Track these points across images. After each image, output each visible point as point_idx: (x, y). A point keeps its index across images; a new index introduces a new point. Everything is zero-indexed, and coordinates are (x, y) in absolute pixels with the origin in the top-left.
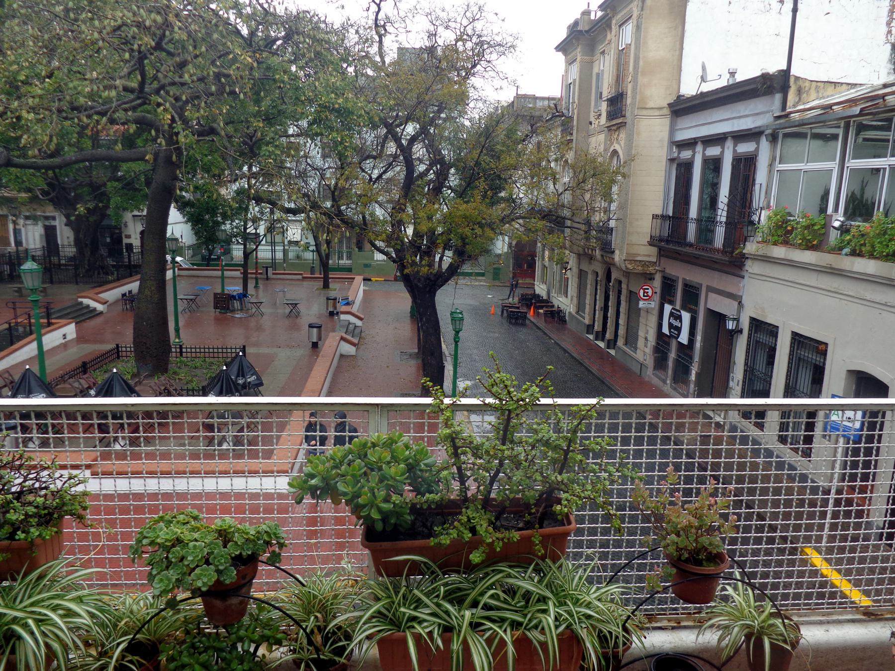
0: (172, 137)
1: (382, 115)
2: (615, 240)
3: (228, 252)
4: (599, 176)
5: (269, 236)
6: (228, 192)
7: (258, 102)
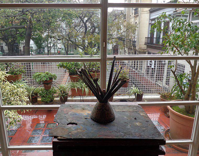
0: (31, 22)
1: (79, 15)
2: (136, 44)
3: (44, 51)
4: (131, 28)
5: (53, 47)
6: (44, 35)
7: (50, 13)
